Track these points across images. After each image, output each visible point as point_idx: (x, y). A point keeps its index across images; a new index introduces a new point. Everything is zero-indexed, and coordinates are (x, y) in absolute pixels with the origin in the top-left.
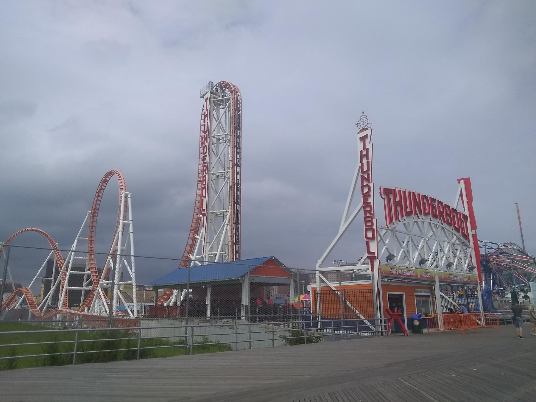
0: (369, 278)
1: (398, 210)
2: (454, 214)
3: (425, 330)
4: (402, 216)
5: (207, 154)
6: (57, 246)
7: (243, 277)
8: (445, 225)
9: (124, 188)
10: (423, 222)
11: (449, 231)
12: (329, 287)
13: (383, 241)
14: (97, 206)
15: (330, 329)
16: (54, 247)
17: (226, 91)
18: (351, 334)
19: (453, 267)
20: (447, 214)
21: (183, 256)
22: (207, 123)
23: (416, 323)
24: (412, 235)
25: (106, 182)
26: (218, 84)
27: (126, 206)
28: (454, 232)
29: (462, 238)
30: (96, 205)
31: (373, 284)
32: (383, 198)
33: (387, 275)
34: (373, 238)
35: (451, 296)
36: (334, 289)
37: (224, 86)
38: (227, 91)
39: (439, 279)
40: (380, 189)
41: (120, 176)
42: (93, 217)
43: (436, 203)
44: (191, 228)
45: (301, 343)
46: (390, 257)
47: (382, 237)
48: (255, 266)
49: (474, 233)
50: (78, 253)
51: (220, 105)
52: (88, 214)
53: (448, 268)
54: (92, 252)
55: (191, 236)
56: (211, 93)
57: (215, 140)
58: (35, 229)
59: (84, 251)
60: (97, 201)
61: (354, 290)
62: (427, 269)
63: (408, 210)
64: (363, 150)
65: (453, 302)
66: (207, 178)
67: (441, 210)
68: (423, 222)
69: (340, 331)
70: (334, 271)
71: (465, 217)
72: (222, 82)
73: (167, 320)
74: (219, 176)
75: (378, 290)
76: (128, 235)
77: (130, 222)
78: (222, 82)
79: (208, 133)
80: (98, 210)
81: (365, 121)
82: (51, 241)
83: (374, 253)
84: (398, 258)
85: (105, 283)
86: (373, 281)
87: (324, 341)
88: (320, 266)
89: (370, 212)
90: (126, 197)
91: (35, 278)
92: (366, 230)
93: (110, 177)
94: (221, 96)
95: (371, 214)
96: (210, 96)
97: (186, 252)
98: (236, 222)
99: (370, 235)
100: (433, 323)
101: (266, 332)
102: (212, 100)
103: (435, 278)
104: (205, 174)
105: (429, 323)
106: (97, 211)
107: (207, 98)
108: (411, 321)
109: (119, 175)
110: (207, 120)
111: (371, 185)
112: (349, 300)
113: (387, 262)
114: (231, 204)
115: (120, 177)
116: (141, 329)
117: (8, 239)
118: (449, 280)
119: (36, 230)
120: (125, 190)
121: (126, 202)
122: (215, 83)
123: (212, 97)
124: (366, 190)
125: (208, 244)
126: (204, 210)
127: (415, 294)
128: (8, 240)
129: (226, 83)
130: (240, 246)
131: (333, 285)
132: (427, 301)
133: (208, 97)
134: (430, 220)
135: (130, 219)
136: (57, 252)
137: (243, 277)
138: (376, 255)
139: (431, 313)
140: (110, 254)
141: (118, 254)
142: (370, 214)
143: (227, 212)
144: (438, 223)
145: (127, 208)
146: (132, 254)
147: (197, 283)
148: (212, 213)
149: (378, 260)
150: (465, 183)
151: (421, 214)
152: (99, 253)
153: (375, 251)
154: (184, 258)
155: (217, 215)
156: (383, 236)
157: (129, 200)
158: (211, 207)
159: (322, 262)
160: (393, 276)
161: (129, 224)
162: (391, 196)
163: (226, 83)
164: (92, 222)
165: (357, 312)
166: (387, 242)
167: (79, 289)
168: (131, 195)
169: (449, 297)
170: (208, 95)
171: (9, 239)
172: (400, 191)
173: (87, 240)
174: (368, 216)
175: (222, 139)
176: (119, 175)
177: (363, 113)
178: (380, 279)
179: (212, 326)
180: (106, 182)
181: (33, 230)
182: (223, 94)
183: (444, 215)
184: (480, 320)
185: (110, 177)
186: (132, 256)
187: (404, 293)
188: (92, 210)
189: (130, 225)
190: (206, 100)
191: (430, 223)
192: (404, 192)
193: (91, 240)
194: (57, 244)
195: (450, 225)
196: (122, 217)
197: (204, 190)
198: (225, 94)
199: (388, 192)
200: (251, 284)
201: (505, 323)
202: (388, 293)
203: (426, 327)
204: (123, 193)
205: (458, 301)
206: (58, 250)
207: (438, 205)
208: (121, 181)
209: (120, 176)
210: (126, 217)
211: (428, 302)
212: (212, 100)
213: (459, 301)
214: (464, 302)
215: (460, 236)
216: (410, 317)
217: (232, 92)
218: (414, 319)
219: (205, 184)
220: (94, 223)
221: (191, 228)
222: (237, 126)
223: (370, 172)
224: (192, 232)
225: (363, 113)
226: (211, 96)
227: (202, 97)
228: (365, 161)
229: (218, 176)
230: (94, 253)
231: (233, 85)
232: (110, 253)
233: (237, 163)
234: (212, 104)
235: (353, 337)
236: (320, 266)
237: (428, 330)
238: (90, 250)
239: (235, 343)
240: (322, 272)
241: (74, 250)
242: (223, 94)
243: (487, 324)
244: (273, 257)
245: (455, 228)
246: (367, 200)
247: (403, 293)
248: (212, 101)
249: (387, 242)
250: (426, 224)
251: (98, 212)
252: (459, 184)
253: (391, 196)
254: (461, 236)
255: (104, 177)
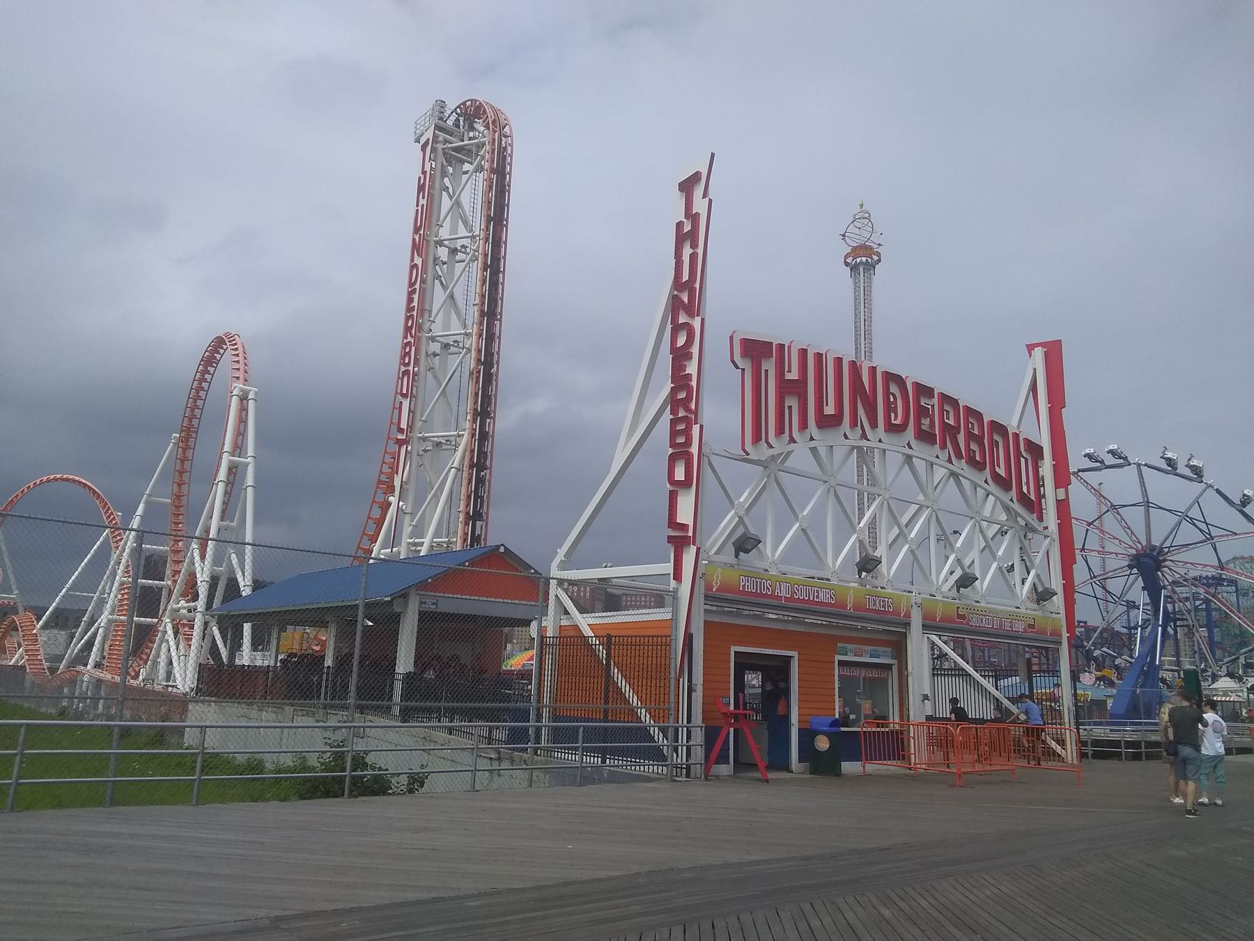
0: (658, 600)
1: (790, 407)
2: (996, 437)
3: (848, 767)
4: (804, 425)
5: (417, 286)
6: (117, 520)
7: (404, 595)
8: (961, 466)
9: (241, 376)
10: (884, 451)
11: (975, 486)
12: (576, 628)
13: (991, 550)
14: (195, 422)
15: (572, 749)
16: (111, 521)
17: (476, 126)
18: (612, 769)
19: (979, 587)
20: (970, 436)
21: (359, 548)
22: (423, 205)
23: (823, 743)
24: (838, 484)
25: (215, 363)
26: (459, 107)
27: (242, 421)
28: (992, 487)
29: (1016, 506)
30: (190, 420)
31: (674, 619)
32: (738, 368)
33: (730, 596)
34: (686, 484)
35: (953, 673)
36: (588, 632)
37: (472, 112)
38: (479, 126)
39: (924, 618)
40: (731, 338)
41: (236, 347)
42: (184, 450)
43: (935, 401)
44: (379, 477)
45: (328, 794)
46: (745, 544)
47: (904, 528)
48: (445, 567)
49: (1062, 496)
50: (259, 549)
51: (462, 162)
52: (173, 441)
53: (864, 574)
54: (179, 533)
55: (380, 498)
56: (437, 127)
57: (443, 253)
58: (71, 477)
59: (273, 545)
60: (193, 410)
61: (628, 637)
62: (978, 602)
63: (830, 410)
64: (685, 220)
65: (994, 689)
66: (413, 348)
67: (951, 422)
68: (884, 451)
69: (596, 758)
70: (594, 581)
71: (1035, 450)
72: (468, 101)
73: (236, 705)
74: (448, 344)
75: (689, 638)
76: (243, 491)
77: (249, 460)
78: (468, 101)
79: (422, 232)
80: (197, 432)
81: (866, 228)
82: (105, 507)
83: (684, 527)
84: (983, 585)
85: (184, 608)
86: (675, 612)
87: (547, 785)
88: (563, 566)
89: (685, 403)
90: (243, 398)
91: (61, 594)
92: (672, 460)
93: (222, 351)
94: (466, 138)
95: (688, 409)
96: (435, 136)
97: (366, 538)
98: (479, 463)
99: (680, 474)
100: (894, 746)
101: (424, 750)
102: (440, 146)
103: (908, 615)
104: (410, 339)
105: (865, 741)
106: (194, 435)
107: (427, 143)
108: (807, 736)
109: (236, 344)
110: (423, 198)
111: (696, 323)
112: (620, 666)
113: (958, 592)
114: (469, 417)
115: (237, 349)
116: (206, 727)
117: (10, 499)
118: (962, 623)
119: (74, 481)
120: (246, 380)
121: (243, 409)
122: (451, 105)
123: (441, 139)
124: (681, 341)
125: (407, 518)
126: (401, 430)
127: (838, 658)
128: (10, 502)
129: (478, 103)
130: (486, 526)
131: (585, 623)
132: (885, 681)
133: (429, 139)
134: (910, 447)
135: (250, 452)
136: (117, 533)
137: (404, 595)
138: (690, 534)
139: (894, 718)
140: (196, 538)
141: (211, 536)
142: (686, 411)
143: (459, 436)
144: (937, 457)
145: (245, 425)
146: (249, 539)
147: (285, 612)
148: (425, 439)
149: (693, 549)
150: (1047, 356)
151: (874, 425)
152: (274, 548)
153: (690, 523)
154: (360, 553)
155: (438, 444)
156: (992, 539)
157: (251, 404)
158: (422, 425)
159: (568, 555)
160: (752, 599)
161: (247, 465)
162: (769, 366)
163: (478, 103)
164: (183, 461)
165: (635, 701)
166: (1000, 553)
167: (144, 621)
168: (256, 393)
169: (984, 677)
170: (429, 135)
171: (12, 500)
172: (803, 353)
173: (166, 504)
174: (680, 415)
175: (463, 250)
176: (236, 344)
177: (861, 206)
178: (700, 605)
179: (319, 727)
180: (215, 363)
181: (67, 480)
182: (471, 134)
183: (961, 438)
184: (1061, 742)
185: (222, 351)
186: (249, 544)
187: (797, 653)
188: (182, 431)
189: (248, 466)
190: (424, 148)
191: (909, 458)
192: (839, 361)
193: (177, 504)
194: (117, 516)
195: (979, 466)
196: (227, 447)
197: (405, 380)
198: (477, 133)
199: (755, 350)
200: (424, 617)
201: (1234, 751)
202: (734, 649)
203: (855, 757)
204: (238, 387)
205: (1039, 691)
206: (120, 529)
207: (942, 411)
208: (237, 359)
209: (236, 347)
210: (238, 448)
211: (887, 684)
212: (440, 146)
213: (1048, 691)
214: (1011, 693)
215: (1011, 500)
216: (807, 726)
217: (487, 127)
218: (817, 733)
219: (408, 364)
220: (187, 465)
221: (379, 477)
222: (497, 217)
223: (697, 286)
224: (381, 488)
225: (861, 206)
226: (438, 138)
227: (418, 141)
228: (687, 251)
229: (446, 346)
230: (183, 536)
231: (493, 108)
232: (196, 535)
233: (491, 310)
234: (441, 158)
235: (616, 778)
236: (563, 566)
237: (864, 767)
238: (174, 530)
239: (472, 771)
240: (561, 582)
241: (135, 527)
242: (471, 134)
243: (1082, 755)
244: (502, 547)
245: (997, 478)
246: (684, 368)
247: (795, 654)
248: (440, 151)
249: (1000, 553)
250: (894, 459)
251: (196, 439)
252: (1030, 356)
253: (769, 366)
254: (1015, 500)
255: (206, 351)
